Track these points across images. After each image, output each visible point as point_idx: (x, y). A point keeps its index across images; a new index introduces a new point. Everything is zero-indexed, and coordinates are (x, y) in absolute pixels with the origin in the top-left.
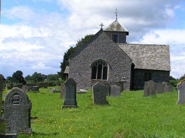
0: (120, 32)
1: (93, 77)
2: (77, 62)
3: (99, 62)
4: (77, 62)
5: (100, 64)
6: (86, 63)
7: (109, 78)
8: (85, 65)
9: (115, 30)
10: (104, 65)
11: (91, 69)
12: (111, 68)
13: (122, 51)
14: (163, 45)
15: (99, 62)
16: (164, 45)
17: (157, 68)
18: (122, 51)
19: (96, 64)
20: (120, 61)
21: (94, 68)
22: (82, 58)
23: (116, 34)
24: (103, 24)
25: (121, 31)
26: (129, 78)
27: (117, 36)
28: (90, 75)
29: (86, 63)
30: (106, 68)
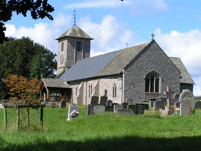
0: (85, 38)
1: (147, 90)
2: (132, 73)
3: (151, 74)
4: (132, 73)
5: (152, 76)
6: (140, 74)
7: (162, 91)
8: (139, 77)
9: (79, 35)
10: (156, 77)
11: (145, 82)
12: (162, 80)
13: (172, 63)
14: (175, 57)
15: (151, 74)
16: (176, 58)
17: (183, 81)
18: (172, 63)
19: (149, 75)
20: (171, 73)
21: (147, 80)
22: (136, 70)
23: (80, 41)
24: (154, 35)
25: (86, 37)
26: (178, 91)
27: (80, 43)
28: (144, 88)
29: (140, 74)
30: (157, 81)
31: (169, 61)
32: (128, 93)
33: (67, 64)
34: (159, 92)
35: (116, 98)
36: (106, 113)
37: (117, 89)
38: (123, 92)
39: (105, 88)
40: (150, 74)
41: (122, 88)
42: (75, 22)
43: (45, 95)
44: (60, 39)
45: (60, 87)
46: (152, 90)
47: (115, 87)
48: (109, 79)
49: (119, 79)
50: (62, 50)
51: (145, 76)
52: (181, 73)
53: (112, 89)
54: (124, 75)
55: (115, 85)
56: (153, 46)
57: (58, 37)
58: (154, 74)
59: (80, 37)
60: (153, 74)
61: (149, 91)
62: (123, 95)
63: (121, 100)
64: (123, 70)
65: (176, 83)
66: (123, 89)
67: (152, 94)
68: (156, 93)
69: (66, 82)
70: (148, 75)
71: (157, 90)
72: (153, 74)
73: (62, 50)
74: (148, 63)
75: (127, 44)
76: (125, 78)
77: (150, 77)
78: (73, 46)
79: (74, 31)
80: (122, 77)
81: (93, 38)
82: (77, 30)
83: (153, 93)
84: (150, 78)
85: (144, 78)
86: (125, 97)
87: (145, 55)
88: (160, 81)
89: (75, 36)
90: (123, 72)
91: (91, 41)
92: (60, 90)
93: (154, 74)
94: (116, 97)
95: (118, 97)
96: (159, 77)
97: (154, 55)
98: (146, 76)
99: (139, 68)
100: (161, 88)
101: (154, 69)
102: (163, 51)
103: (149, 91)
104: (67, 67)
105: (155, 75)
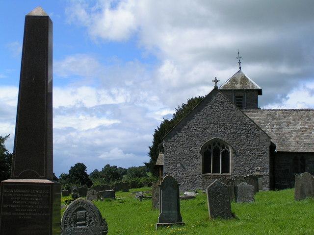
1: (206, 169)
3: (214, 144)
8: (191, 149)
11: (201, 156)
12: (234, 153)
15: (214, 144)
21: (206, 155)
22: (185, 139)
23: (241, 94)
25: (248, 88)
26: (267, 169)
27: (242, 97)
28: (200, 167)
36: (270, 192)
40: (212, 145)
42: (240, 68)
43: (160, 171)
60: (216, 145)
65: (261, 155)
68: (213, 174)
71: (226, 169)
72: (216, 145)
83: (217, 174)
87: (202, 113)
96: (228, 148)
100: (233, 165)
101: (217, 135)
105: (221, 145)
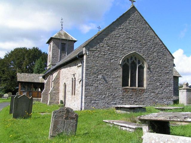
1: (125, 83)
2: (100, 55)
4: (100, 55)
6: (113, 57)
8: (112, 61)
9: (64, 38)
10: (139, 63)
11: (121, 70)
12: (149, 68)
19: (128, 60)
20: (160, 59)
21: (125, 67)
22: (107, 49)
23: (65, 42)
25: (70, 39)
27: (65, 44)
28: (120, 80)
29: (113, 57)
30: (141, 68)
31: (158, 40)
32: (92, 88)
33: (52, 62)
34: (143, 87)
35: (75, 97)
37: (76, 82)
38: (84, 87)
39: (64, 81)
40: (129, 59)
41: (82, 80)
44: (49, 42)
45: (33, 81)
46: (133, 84)
47: (74, 80)
48: (69, 68)
49: (79, 65)
50: (50, 51)
51: (121, 61)
52: (174, 58)
53: (71, 82)
54: (85, 57)
55: (74, 75)
56: (133, 15)
57: (47, 40)
58: (135, 58)
59: (64, 39)
60: (134, 59)
61: (128, 86)
62: (84, 91)
63: (81, 99)
64: (84, 49)
66: (84, 81)
67: (133, 89)
69: (41, 77)
70: (126, 60)
71: (141, 84)
72: (134, 59)
73: (50, 51)
74: (126, 40)
75: (99, 28)
76: (87, 62)
77: (130, 62)
78: (58, 46)
79: (60, 34)
80: (82, 62)
81: (76, 40)
82: (63, 34)
83: (134, 88)
84: (129, 64)
85: (121, 63)
86: (86, 96)
87: (122, 27)
88: (145, 70)
89: (60, 38)
90: (84, 53)
91: (75, 44)
92: (33, 85)
93: (135, 58)
94: (75, 95)
95: (77, 94)
96: (143, 64)
97: (135, 30)
98: (124, 61)
99: (112, 48)
100: (147, 80)
102: (148, 25)
103: (128, 86)
104: (52, 65)
105: (137, 60)
